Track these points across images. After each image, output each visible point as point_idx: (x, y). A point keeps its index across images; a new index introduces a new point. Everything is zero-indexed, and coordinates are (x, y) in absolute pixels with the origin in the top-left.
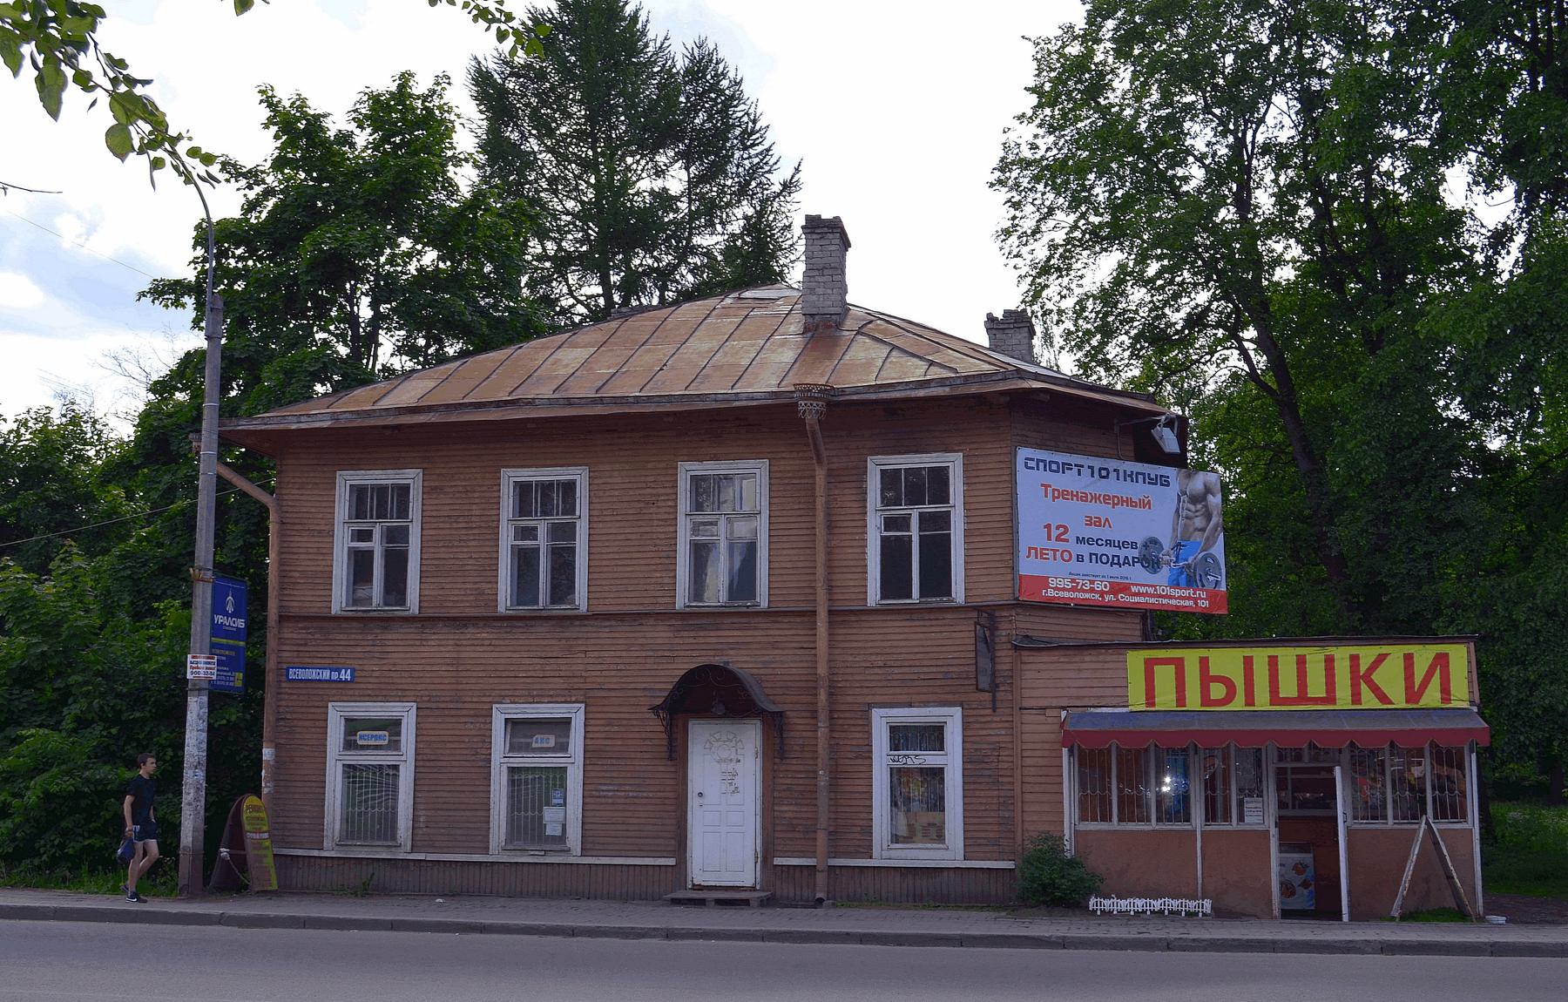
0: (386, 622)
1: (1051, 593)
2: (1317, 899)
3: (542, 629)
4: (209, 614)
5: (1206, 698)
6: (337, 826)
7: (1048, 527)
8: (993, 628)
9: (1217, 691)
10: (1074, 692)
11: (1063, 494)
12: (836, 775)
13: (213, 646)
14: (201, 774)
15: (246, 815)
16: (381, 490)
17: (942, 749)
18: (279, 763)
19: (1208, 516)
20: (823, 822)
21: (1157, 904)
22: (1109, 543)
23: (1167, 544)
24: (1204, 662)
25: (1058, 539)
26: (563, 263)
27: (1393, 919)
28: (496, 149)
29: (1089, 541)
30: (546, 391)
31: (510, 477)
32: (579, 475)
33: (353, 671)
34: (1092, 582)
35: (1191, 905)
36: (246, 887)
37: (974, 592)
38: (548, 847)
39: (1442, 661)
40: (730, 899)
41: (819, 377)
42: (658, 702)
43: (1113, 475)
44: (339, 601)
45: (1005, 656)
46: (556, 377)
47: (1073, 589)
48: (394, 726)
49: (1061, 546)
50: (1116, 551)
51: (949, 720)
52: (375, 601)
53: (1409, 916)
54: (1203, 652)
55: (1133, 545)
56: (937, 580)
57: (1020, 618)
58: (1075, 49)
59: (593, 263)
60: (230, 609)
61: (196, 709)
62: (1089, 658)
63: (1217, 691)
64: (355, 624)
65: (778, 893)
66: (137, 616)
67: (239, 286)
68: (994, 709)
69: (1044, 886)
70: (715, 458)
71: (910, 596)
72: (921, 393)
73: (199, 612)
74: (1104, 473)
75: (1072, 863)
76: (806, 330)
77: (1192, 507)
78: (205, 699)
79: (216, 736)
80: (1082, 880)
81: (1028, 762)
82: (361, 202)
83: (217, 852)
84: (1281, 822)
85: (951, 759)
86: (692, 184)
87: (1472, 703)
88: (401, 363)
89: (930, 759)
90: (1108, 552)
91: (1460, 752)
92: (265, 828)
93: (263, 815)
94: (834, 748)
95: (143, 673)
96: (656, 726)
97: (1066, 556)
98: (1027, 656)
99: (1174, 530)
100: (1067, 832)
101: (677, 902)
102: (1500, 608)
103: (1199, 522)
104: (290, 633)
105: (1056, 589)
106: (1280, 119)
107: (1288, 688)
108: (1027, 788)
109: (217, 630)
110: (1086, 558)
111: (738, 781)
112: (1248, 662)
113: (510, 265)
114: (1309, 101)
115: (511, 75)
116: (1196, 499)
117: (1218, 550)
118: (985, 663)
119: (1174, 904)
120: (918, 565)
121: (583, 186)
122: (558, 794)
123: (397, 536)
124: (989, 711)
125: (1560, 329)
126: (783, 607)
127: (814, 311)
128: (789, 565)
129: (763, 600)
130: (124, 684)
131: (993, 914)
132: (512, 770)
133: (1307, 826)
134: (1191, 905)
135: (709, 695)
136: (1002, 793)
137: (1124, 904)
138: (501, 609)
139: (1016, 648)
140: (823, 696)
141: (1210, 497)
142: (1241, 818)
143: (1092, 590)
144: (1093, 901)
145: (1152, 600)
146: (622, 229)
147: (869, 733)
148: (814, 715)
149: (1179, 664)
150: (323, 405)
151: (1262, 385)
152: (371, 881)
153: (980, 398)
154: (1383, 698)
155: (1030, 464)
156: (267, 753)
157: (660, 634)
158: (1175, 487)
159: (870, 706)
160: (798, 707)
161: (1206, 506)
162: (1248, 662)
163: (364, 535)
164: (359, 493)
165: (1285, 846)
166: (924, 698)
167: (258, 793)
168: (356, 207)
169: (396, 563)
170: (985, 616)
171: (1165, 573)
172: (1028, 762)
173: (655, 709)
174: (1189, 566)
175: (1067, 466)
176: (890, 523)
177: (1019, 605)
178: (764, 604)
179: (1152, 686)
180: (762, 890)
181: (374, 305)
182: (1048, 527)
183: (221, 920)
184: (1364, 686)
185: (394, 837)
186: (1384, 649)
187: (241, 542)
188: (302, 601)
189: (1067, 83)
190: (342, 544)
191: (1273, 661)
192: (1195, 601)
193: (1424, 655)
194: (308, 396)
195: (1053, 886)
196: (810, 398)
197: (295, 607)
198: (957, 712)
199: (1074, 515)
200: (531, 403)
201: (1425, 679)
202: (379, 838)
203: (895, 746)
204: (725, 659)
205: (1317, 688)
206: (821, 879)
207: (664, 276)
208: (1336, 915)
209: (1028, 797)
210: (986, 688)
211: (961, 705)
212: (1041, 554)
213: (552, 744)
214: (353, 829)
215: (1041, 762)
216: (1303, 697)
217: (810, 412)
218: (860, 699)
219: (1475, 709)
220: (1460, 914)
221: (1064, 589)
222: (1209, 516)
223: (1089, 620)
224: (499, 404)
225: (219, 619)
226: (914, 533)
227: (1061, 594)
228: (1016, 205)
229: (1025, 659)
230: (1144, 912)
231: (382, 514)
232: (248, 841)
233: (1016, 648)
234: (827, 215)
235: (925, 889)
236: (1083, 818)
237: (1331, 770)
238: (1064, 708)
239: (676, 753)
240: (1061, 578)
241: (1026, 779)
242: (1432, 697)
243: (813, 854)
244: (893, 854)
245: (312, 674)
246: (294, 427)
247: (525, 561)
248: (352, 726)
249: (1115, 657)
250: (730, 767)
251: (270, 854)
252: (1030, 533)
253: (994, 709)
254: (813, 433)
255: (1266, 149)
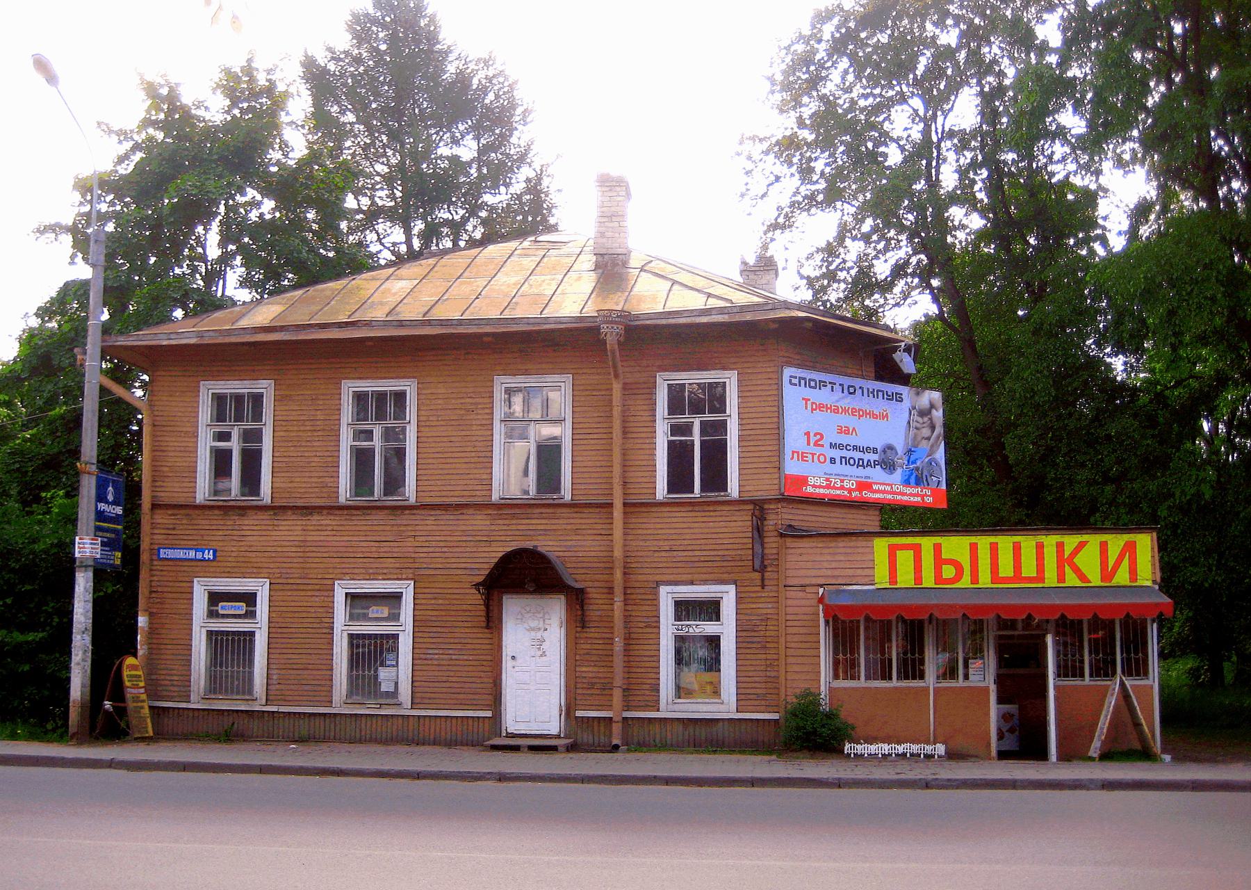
0: (243, 510)
1: (810, 490)
2: (1026, 741)
3: (381, 515)
4: (93, 501)
5: (938, 577)
6: (202, 683)
7: (808, 434)
8: (762, 519)
9: (949, 571)
10: (829, 573)
11: (821, 407)
12: (628, 639)
13: (98, 529)
14: (88, 639)
15: (126, 673)
16: (239, 399)
17: (718, 619)
18: (152, 631)
19: (933, 428)
20: (618, 681)
21: (900, 749)
22: (855, 448)
23: (900, 448)
24: (938, 548)
25: (816, 444)
26: (373, 214)
27: (1091, 759)
28: (321, 120)
29: (840, 446)
30: (379, 314)
31: (349, 388)
32: (410, 387)
33: (215, 552)
34: (842, 481)
35: (929, 749)
36: (128, 734)
37: (748, 488)
38: (382, 701)
39: (1130, 548)
40: (541, 746)
41: (616, 303)
42: (481, 579)
43: (859, 392)
44: (203, 489)
45: (772, 542)
46: (386, 303)
47: (828, 487)
48: (250, 599)
49: (818, 451)
50: (860, 455)
51: (725, 596)
52: (233, 493)
53: (1106, 756)
54: (938, 540)
55: (875, 451)
56: (715, 476)
57: (784, 510)
58: (800, 48)
59: (401, 217)
60: (110, 498)
61: (83, 584)
62: (842, 543)
63: (949, 571)
64: (217, 512)
65: (579, 740)
66: (25, 503)
67: (110, 227)
68: (763, 586)
69: (808, 733)
70: (526, 373)
71: (693, 492)
72: (704, 320)
73: (85, 500)
74: (852, 390)
75: (830, 716)
76: (597, 266)
77: (920, 419)
78: (91, 574)
79: (100, 606)
80: (839, 730)
81: (790, 630)
82: (216, 157)
83: (102, 705)
84: (1000, 680)
85: (726, 628)
86: (482, 151)
87: (1154, 582)
88: (244, 295)
89: (709, 628)
90: (854, 456)
91: (1144, 622)
92: (142, 684)
93: (140, 673)
94: (627, 619)
95: (33, 552)
96: (476, 598)
97: (821, 459)
98: (789, 541)
99: (906, 437)
100: (822, 688)
101: (495, 748)
102: (1144, 505)
103: (926, 432)
104: (162, 518)
105: (814, 486)
106: (965, 111)
107: (1006, 570)
108: (790, 652)
109: (100, 516)
110: (838, 461)
111: (545, 646)
112: (974, 547)
113: (331, 212)
114: (988, 99)
115: (333, 59)
116: (922, 413)
117: (940, 454)
118: (758, 548)
119: (915, 748)
120: (696, 467)
121: (390, 153)
122: (391, 656)
123: (252, 437)
124: (759, 589)
125: (1197, 282)
126: (583, 499)
127: (603, 251)
128: (590, 464)
129: (567, 493)
130: (18, 561)
131: (767, 758)
132: (351, 636)
133: (1020, 685)
134: (929, 749)
135: (523, 574)
136: (769, 657)
137: (873, 748)
138: (342, 500)
139: (782, 535)
140: (618, 575)
141: (934, 411)
142: (966, 677)
143: (842, 488)
144: (847, 746)
145: (890, 497)
146: (424, 191)
147: (657, 606)
148: (610, 590)
149: (917, 549)
150: (181, 326)
151: (951, 326)
152: (230, 729)
153: (752, 325)
154: (1082, 577)
155: (794, 381)
156: (142, 621)
157: (479, 522)
158: (907, 404)
159: (658, 584)
160: (596, 584)
161: (931, 419)
162: (974, 547)
163: (224, 436)
164: (219, 400)
165: (1000, 701)
166: (704, 577)
167: (135, 655)
168: (211, 161)
169: (252, 460)
170: (758, 508)
171: (898, 476)
172: (790, 630)
173: (477, 586)
174: (917, 469)
175: (822, 384)
176: (675, 429)
177: (785, 500)
178: (568, 497)
179: (897, 569)
180: (565, 737)
181: (223, 243)
182: (808, 434)
183: (111, 764)
184: (1067, 568)
185: (250, 692)
186: (1085, 537)
187: (113, 442)
188: (172, 492)
189: (803, 76)
190: (205, 444)
191: (994, 548)
192: (922, 497)
193: (1116, 543)
194: (168, 319)
195: (813, 734)
196: (612, 322)
197: (165, 497)
198: (731, 589)
199: (828, 425)
200: (368, 324)
201: (1114, 563)
202: (238, 693)
203: (678, 618)
204: (535, 543)
205: (1029, 570)
206: (617, 728)
207: (456, 228)
208: (1042, 755)
209: (790, 660)
210: (757, 568)
211: (735, 582)
212: (803, 457)
213: (386, 614)
214: (215, 684)
215: (802, 630)
216: (1018, 576)
217: (611, 335)
218: (651, 578)
219: (1157, 587)
220: (1145, 754)
221: (820, 487)
222: (933, 428)
223: (838, 513)
224: (341, 325)
225: (102, 506)
226: (697, 438)
227: (817, 490)
228: (748, 173)
229: (788, 545)
230: (890, 755)
231: (239, 418)
232: (128, 696)
233: (782, 535)
234: (615, 173)
235: (704, 736)
236: (836, 677)
237: (1044, 636)
238: (821, 586)
239: (492, 622)
240: (819, 477)
241: (789, 645)
242: (1122, 577)
243: (609, 707)
244: (676, 707)
245: (180, 554)
246: (165, 343)
247: (362, 459)
248: (215, 598)
249: (864, 544)
250: (539, 635)
251: (146, 705)
252: (794, 439)
253: (763, 586)
254: (613, 352)
255: (951, 134)
